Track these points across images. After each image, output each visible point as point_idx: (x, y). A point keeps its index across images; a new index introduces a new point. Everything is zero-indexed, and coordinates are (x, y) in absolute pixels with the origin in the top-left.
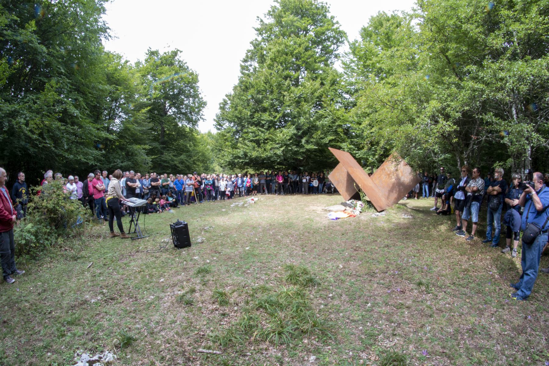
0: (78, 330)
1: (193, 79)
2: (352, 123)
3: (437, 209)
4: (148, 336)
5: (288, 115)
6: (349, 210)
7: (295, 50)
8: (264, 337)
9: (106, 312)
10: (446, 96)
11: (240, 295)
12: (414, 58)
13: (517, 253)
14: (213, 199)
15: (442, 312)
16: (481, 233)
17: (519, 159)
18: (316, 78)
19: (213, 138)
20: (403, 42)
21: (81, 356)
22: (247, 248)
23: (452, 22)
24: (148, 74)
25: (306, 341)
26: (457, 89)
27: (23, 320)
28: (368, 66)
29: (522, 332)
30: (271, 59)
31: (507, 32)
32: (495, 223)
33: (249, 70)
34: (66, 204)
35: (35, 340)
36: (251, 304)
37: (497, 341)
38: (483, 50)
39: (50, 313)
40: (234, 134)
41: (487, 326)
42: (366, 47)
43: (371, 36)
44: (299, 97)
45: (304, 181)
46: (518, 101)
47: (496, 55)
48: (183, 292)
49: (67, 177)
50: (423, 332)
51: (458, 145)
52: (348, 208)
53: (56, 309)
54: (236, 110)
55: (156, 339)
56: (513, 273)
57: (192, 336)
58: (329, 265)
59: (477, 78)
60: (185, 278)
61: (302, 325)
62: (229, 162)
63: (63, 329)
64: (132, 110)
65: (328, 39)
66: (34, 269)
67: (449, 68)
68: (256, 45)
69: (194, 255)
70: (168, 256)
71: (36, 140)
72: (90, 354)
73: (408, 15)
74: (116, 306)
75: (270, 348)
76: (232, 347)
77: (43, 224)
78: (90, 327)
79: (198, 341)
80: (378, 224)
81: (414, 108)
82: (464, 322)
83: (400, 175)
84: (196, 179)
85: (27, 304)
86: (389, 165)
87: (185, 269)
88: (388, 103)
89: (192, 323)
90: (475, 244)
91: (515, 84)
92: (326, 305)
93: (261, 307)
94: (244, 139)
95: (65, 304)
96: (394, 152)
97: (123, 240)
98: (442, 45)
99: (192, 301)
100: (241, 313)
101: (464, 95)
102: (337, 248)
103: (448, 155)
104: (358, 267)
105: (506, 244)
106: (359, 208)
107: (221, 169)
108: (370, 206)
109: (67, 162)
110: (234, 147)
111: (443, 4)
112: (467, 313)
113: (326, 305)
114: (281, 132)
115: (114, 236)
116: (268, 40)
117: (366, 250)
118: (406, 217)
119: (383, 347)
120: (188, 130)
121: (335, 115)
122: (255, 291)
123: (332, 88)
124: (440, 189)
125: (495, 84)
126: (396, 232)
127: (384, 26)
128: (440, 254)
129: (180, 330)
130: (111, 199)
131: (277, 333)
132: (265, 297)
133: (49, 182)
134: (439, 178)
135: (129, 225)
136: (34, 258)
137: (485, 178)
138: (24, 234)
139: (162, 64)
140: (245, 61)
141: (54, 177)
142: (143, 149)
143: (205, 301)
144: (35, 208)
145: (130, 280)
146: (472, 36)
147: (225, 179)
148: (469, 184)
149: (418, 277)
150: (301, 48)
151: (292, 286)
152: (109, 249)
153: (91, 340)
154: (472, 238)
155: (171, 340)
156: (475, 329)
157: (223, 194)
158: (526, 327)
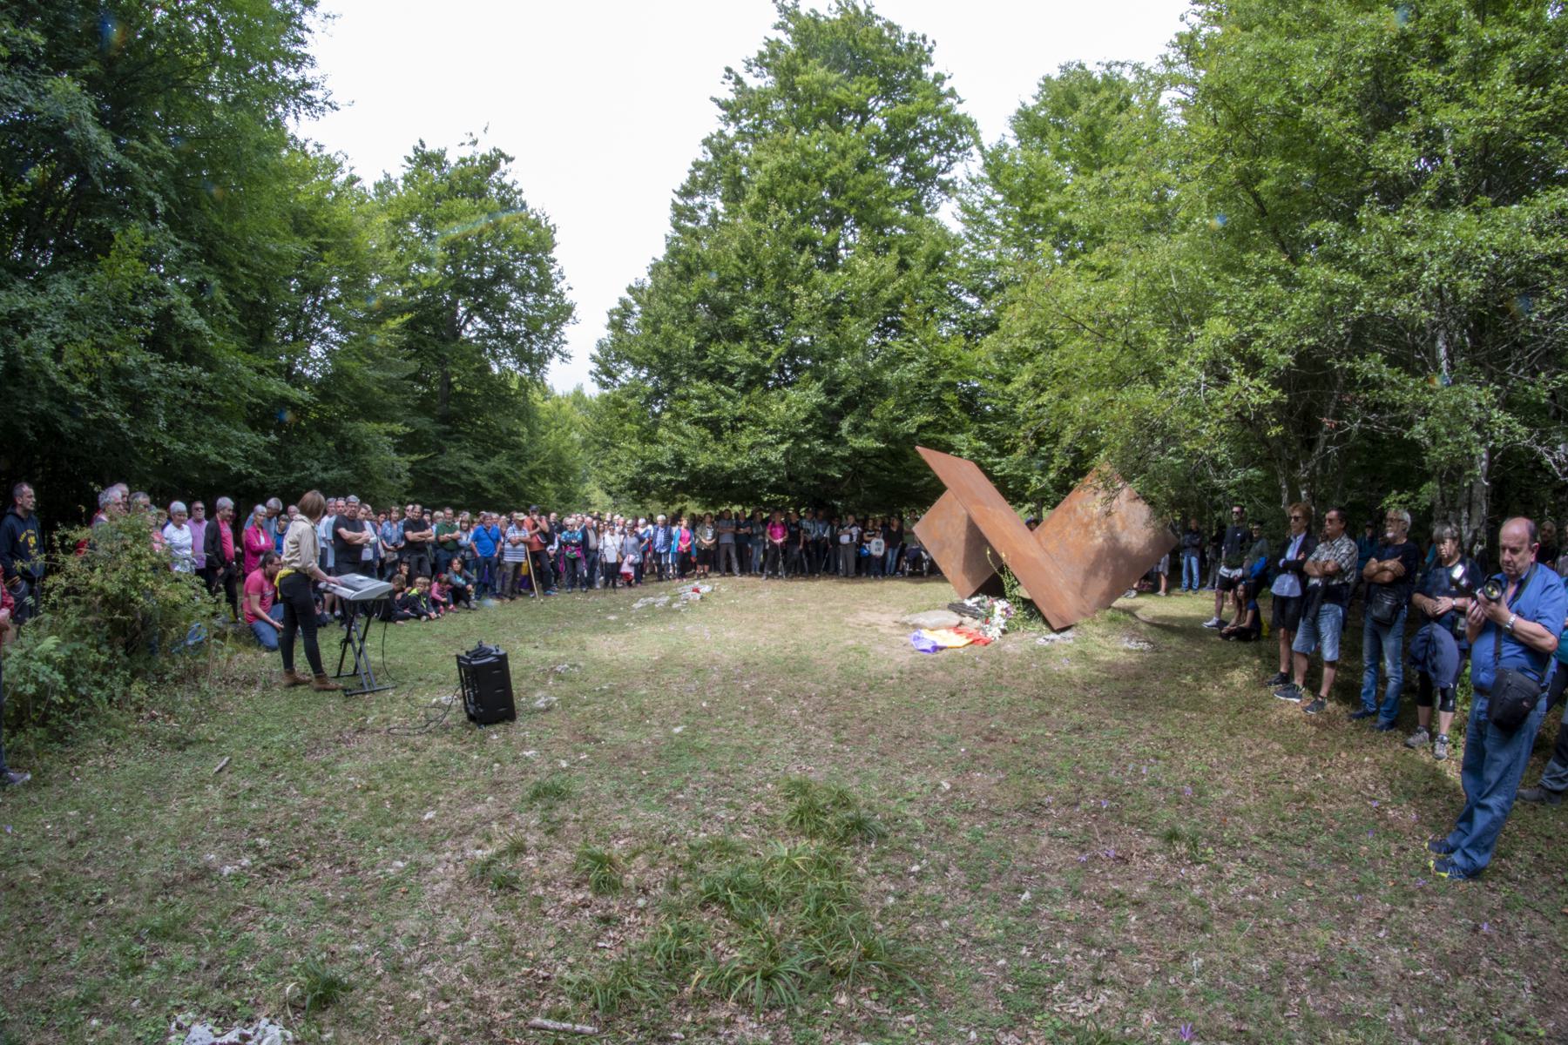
0: (181, 955)
1: (538, 239)
2: (983, 377)
3: (1222, 623)
4: (387, 979)
5: (803, 351)
6: (971, 624)
7: (828, 166)
8: (722, 988)
9: (264, 905)
10: (1251, 306)
11: (653, 865)
12: (1162, 198)
13: (1450, 746)
14: (582, 585)
15: (1237, 915)
16: (1346, 691)
17: (1454, 482)
18: (888, 247)
19: (588, 408)
20: (1135, 153)
21: (187, 1030)
22: (677, 730)
23: (1272, 100)
24: (411, 219)
25: (843, 1000)
26: (1285, 285)
27: (20, 918)
28: (1035, 217)
29: (1465, 968)
30: (760, 190)
31: (1427, 129)
32: (1388, 665)
33: (696, 219)
34: (158, 583)
35: (56, 980)
36: (686, 892)
37: (1395, 996)
38: (1360, 179)
39: (100, 901)
40: (647, 401)
41: (1366, 954)
42: (1032, 165)
43: (1043, 134)
44: (837, 301)
45: (845, 539)
46: (1453, 323)
47: (1395, 192)
48: (490, 851)
49: (166, 506)
50: (1181, 975)
51: (1285, 444)
52: (968, 619)
53: (119, 891)
54: (656, 331)
55: (407, 987)
56: (1439, 804)
57: (514, 980)
58: (913, 780)
59: (1339, 257)
60: (495, 811)
61: (831, 952)
62: (632, 479)
63: (136, 948)
64: (361, 321)
65: (925, 138)
66: (59, 769)
67: (1262, 226)
68: (719, 147)
69: (524, 745)
70: (450, 746)
71: (79, 397)
72: (216, 1024)
73: (1152, 77)
74: (293, 886)
75: (740, 1019)
76: (628, 1014)
77: (89, 640)
78: (217, 947)
79: (529, 996)
80: (1055, 667)
81: (1160, 339)
82: (1300, 945)
83: (1118, 528)
84: (535, 526)
85: (34, 873)
86: (1086, 501)
87: (497, 784)
88: (1089, 325)
89: (513, 942)
90: (1329, 723)
91: (1447, 273)
92: (901, 897)
93: (714, 899)
94: (677, 416)
95: (145, 875)
96: (1103, 463)
97: (320, 695)
98: (1244, 163)
99: (516, 880)
100: (657, 916)
101: (1302, 304)
102: (936, 733)
103: (1254, 473)
104: (995, 789)
105: (1417, 723)
106: (998, 620)
107: (609, 500)
108: (1032, 615)
109: (166, 461)
110: (648, 437)
111: (1249, 49)
112: (1307, 920)
113: (901, 897)
114: (783, 399)
115: (296, 683)
116: (752, 135)
117: (1018, 739)
118: (1133, 645)
119: (1067, 1018)
120: (514, 385)
121: (937, 353)
122: (699, 852)
123: (930, 277)
124: (1231, 567)
125: (1390, 273)
126: (1105, 689)
127: (1083, 107)
128: (1229, 750)
129: (478, 963)
130: (289, 575)
131: (758, 974)
132: (727, 872)
133: (111, 518)
134: (1228, 536)
135: (339, 652)
136: (60, 738)
137: (1359, 536)
138: (36, 665)
139: (453, 192)
140: (687, 193)
141: (128, 505)
142: (388, 434)
143: (553, 878)
144: (66, 592)
145: (336, 811)
146: (1328, 140)
147: (618, 529)
148: (1315, 555)
149: (1166, 815)
150: (847, 164)
151: (803, 842)
152: (279, 721)
153: (218, 984)
154: (1322, 704)
155: (454, 990)
156: (1332, 964)
157: (613, 572)
158: (1476, 954)
